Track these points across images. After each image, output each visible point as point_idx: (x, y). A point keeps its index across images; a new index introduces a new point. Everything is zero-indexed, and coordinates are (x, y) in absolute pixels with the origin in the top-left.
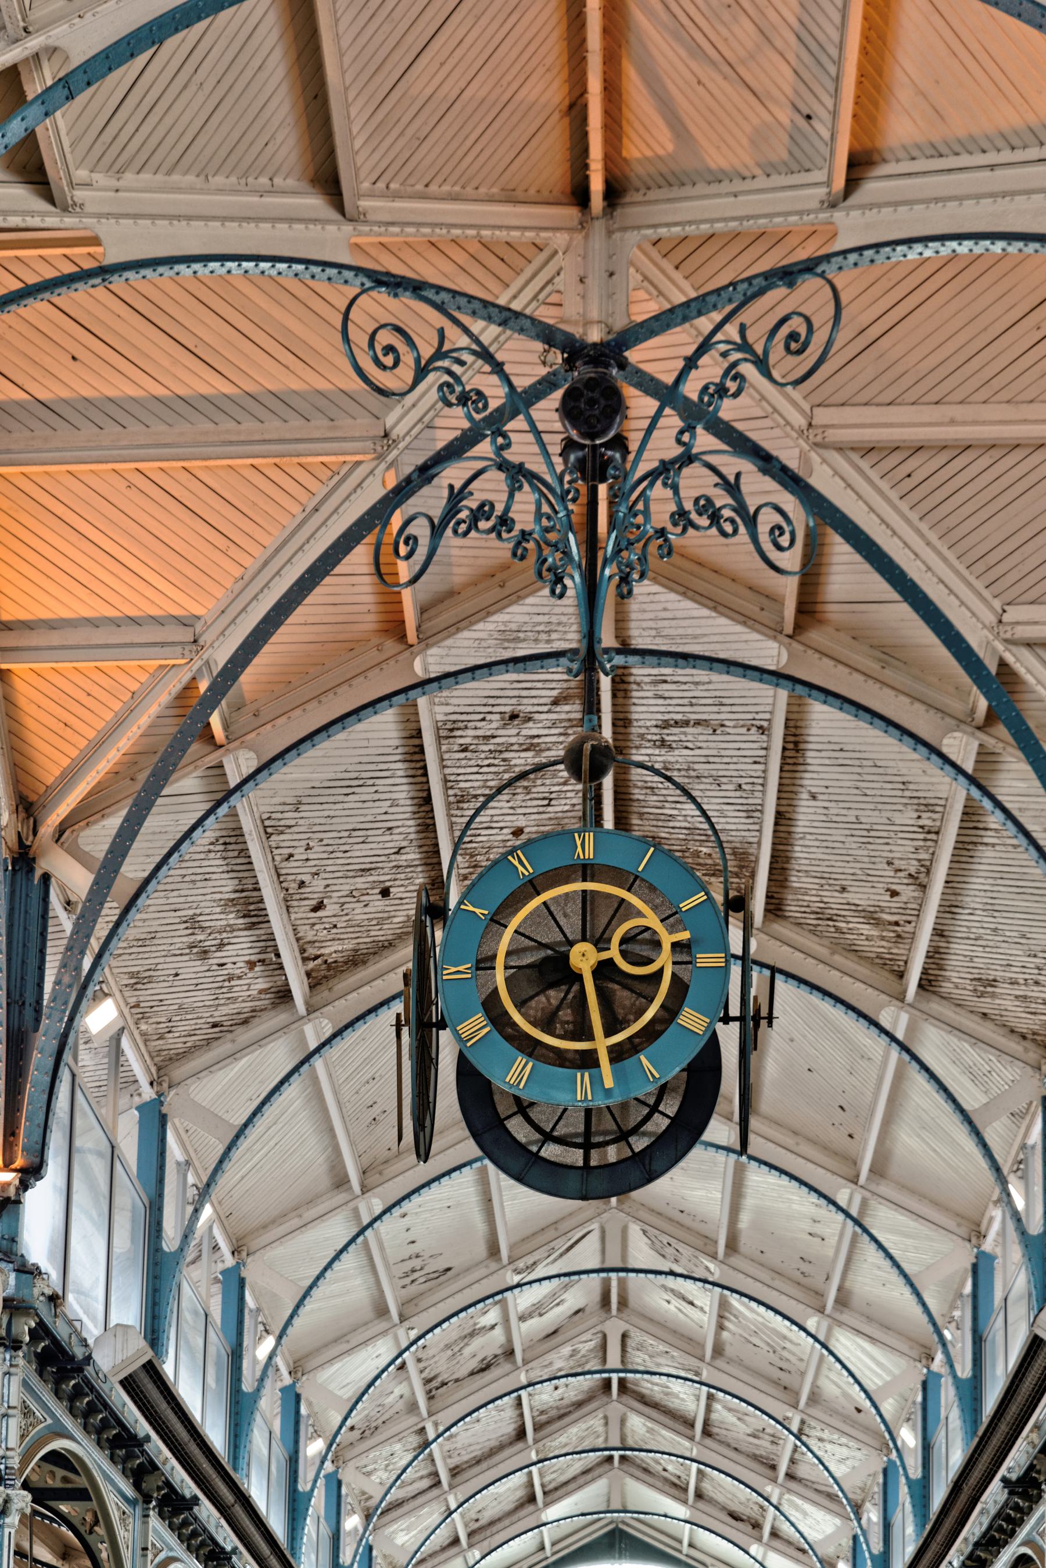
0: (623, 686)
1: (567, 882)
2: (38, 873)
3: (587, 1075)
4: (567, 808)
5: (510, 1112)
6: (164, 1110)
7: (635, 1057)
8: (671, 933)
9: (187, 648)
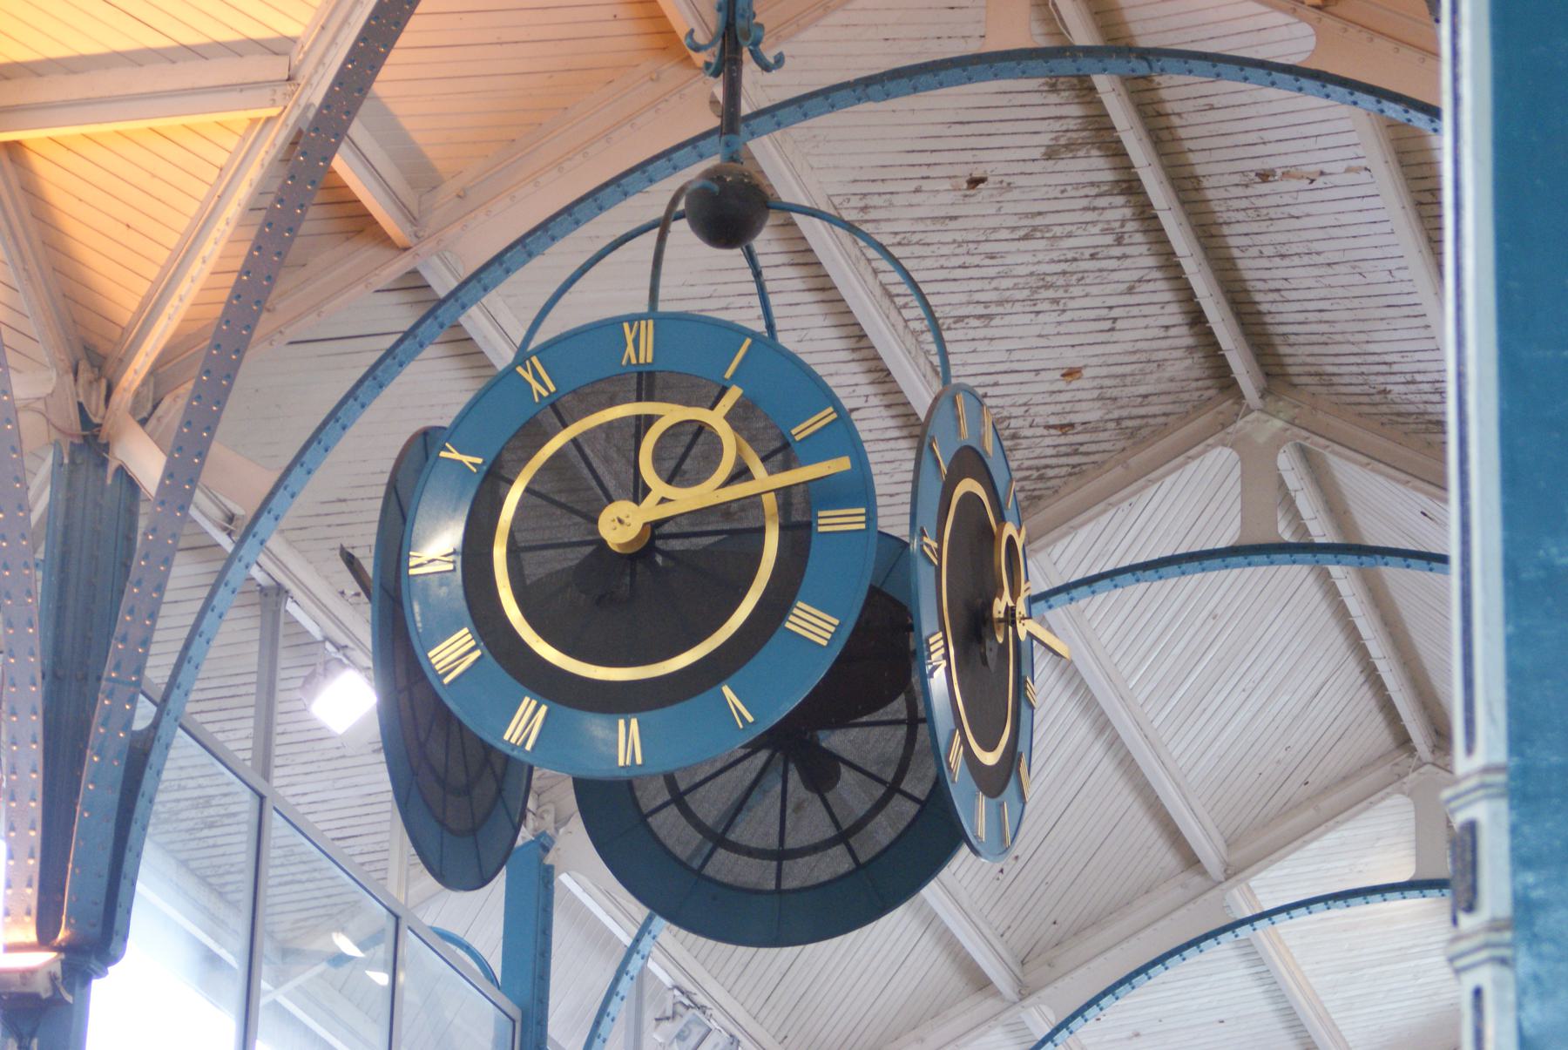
0: (1162, 122)
1: (612, 402)
2: (112, 466)
3: (544, 709)
4: (1151, 333)
5: (659, 802)
6: (549, 859)
7: (715, 689)
8: (770, 473)
9: (280, 90)
